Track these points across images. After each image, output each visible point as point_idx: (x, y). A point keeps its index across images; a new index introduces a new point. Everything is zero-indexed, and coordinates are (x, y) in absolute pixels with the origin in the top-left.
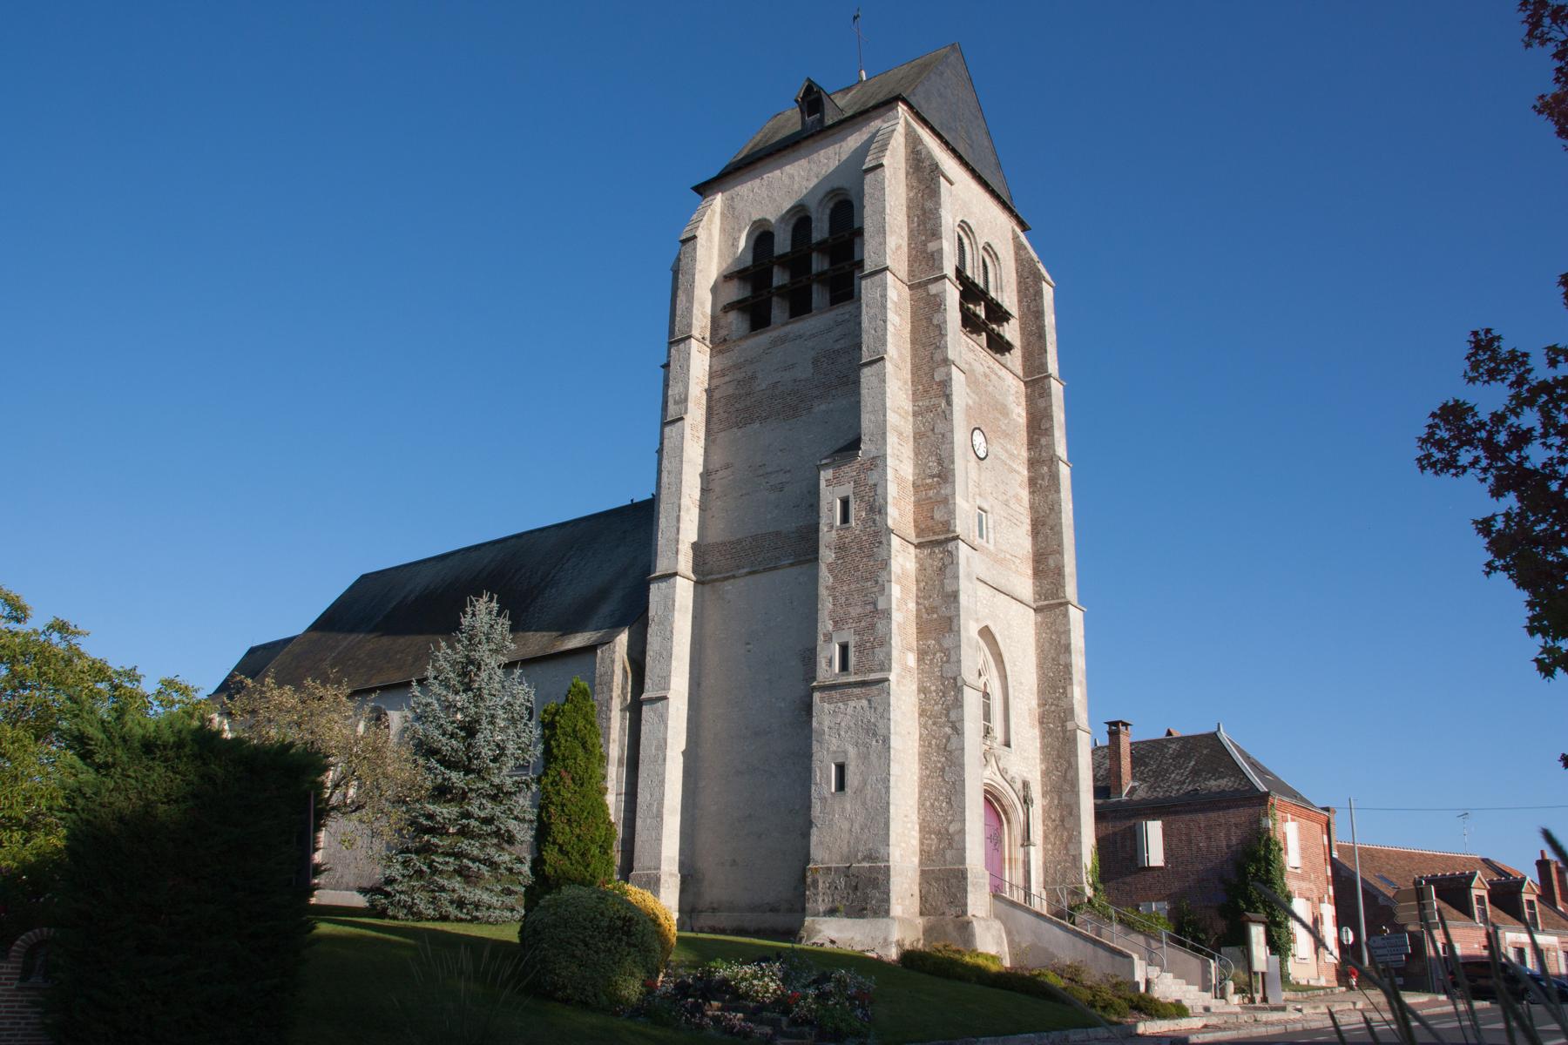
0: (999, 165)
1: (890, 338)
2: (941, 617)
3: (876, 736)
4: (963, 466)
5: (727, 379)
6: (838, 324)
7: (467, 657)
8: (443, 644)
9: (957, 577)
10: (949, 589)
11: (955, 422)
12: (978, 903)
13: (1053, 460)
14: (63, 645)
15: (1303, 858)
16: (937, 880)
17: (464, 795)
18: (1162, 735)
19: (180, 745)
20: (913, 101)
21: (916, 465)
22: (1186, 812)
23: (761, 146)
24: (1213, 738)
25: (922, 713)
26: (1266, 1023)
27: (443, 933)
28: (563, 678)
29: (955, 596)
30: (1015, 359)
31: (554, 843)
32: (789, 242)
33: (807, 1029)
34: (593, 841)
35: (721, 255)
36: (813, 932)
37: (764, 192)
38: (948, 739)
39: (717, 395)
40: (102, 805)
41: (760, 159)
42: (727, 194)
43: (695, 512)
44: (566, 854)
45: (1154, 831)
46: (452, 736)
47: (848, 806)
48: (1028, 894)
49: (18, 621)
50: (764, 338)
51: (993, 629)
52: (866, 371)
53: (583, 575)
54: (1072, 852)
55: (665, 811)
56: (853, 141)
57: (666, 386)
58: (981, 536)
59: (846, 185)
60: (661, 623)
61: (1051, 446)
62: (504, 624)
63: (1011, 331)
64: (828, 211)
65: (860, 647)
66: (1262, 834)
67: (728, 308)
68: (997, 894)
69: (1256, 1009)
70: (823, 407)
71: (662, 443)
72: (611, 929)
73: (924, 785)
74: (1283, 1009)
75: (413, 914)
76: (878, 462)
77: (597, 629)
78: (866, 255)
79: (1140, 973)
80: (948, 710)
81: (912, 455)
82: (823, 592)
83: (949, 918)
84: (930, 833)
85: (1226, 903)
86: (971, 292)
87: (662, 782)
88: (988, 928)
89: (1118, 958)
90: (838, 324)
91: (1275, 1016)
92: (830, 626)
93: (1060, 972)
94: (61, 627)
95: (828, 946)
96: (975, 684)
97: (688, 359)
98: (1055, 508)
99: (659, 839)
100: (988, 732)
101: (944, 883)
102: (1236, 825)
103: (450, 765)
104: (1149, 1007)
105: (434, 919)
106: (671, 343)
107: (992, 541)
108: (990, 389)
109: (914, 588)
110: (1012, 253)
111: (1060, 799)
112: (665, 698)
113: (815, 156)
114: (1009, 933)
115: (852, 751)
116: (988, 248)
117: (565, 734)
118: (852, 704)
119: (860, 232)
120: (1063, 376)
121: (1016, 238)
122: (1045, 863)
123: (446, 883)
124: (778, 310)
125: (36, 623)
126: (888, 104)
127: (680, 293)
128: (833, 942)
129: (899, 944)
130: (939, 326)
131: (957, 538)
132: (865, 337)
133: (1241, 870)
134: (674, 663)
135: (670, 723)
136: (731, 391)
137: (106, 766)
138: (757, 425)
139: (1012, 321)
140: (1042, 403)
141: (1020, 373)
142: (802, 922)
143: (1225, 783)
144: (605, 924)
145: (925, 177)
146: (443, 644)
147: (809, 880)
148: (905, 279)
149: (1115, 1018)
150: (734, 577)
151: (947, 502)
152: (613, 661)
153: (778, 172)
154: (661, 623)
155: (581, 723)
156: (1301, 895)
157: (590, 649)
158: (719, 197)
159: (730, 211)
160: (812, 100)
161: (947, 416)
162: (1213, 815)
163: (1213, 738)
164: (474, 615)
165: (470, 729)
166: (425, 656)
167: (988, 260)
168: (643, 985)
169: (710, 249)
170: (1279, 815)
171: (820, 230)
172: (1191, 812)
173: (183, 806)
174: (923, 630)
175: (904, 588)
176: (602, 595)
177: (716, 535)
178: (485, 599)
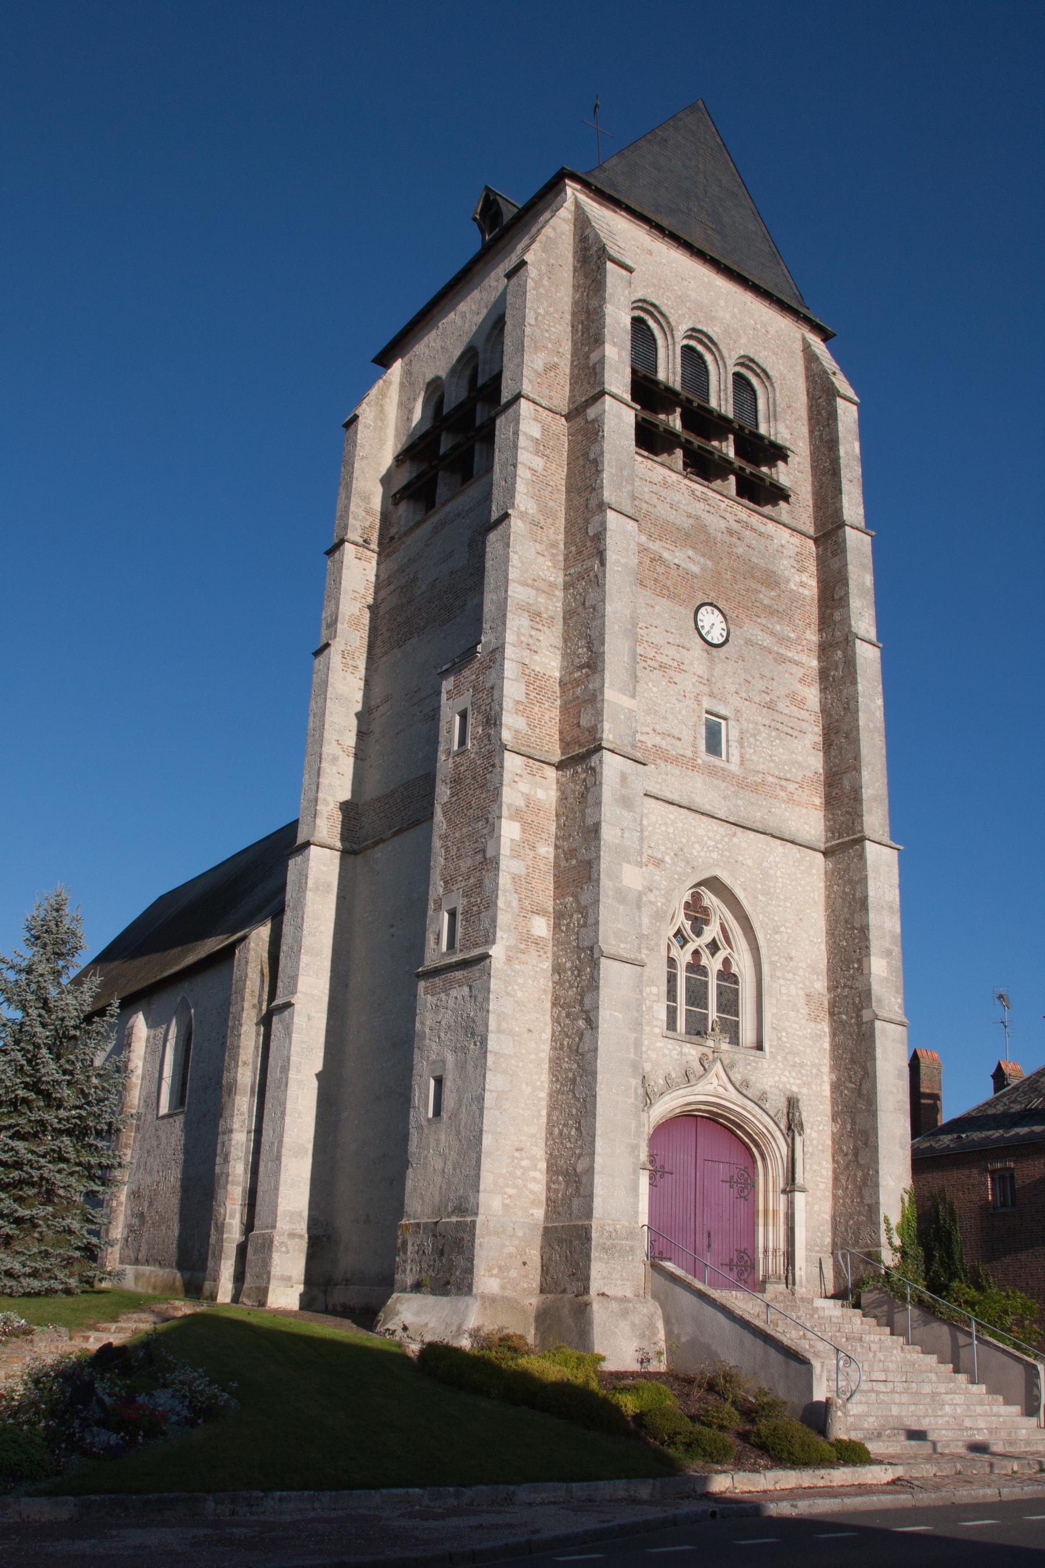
1: (521, 487)
5: (392, 587)
9: (598, 804)
13: (848, 640)
16: (560, 1241)
29: (596, 829)
35: (396, 436)
39: (382, 610)
42: (406, 358)
47: (443, 1137)
54: (867, 1201)
60: (295, 908)
80: (582, 995)
84: (557, 1173)
108: (740, 551)
109: (553, 828)
111: (853, 1123)
113: (486, 283)
115: (450, 1058)
118: (454, 993)
120: (872, 522)
122: (833, 1217)
129: (474, 1334)
138: (415, 640)
140: (834, 563)
153: (452, 315)
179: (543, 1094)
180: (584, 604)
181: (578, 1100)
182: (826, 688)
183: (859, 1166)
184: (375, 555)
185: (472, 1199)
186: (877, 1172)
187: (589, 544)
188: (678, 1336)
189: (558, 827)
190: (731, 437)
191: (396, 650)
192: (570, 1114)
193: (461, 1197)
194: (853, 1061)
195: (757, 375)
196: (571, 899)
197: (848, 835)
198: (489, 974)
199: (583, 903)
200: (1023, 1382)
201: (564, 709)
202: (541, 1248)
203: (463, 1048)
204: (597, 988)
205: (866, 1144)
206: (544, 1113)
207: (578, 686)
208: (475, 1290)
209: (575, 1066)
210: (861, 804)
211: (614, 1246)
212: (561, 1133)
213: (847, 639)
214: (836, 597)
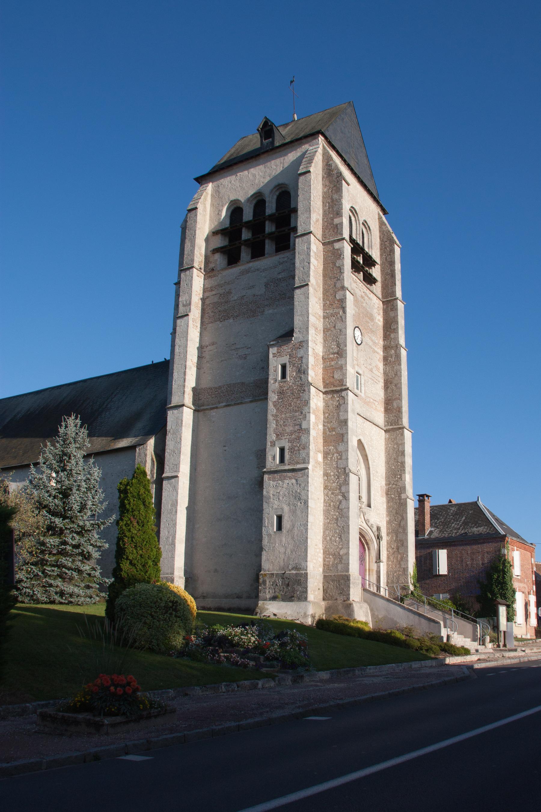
0: (372, 175)
2: (337, 434)
3: (300, 500)
4: (350, 347)
5: (214, 293)
6: (281, 263)
7: (63, 451)
8: (49, 444)
9: (346, 411)
10: (342, 418)
11: (348, 323)
12: (355, 594)
13: (397, 347)
15: (521, 570)
16: (333, 581)
17: (62, 531)
18: (446, 502)
20: (327, 134)
21: (324, 347)
22: (461, 545)
23: (235, 156)
24: (475, 505)
26: (509, 658)
29: (346, 422)
30: (378, 288)
31: (127, 559)
32: (252, 214)
34: (149, 558)
35: (211, 220)
36: (264, 609)
37: (238, 184)
38: (340, 502)
39: (207, 302)
41: (236, 164)
42: (215, 183)
43: (194, 370)
44: (134, 565)
45: (443, 555)
46: (55, 497)
47: (284, 539)
48: (378, 588)
50: (235, 270)
51: (363, 441)
53: (131, 402)
54: (403, 566)
55: (177, 541)
56: (292, 156)
57: (178, 295)
59: (287, 182)
60: (174, 433)
61: (397, 339)
62: (84, 432)
63: (376, 272)
64: (275, 197)
65: (291, 450)
66: (501, 557)
67: (215, 251)
68: (365, 590)
69: (501, 650)
70: (271, 311)
71: (175, 329)
72: (166, 608)
73: (326, 528)
74: (515, 650)
75: (34, 600)
76: (304, 344)
77: (135, 436)
78: (299, 224)
79: (444, 633)
81: (322, 341)
82: (270, 418)
83: (339, 602)
84: (329, 554)
85: (482, 594)
86: (357, 249)
87: (175, 525)
88: (361, 607)
89: (432, 624)
90: (281, 263)
91: (512, 654)
93: (402, 631)
95: (272, 617)
97: (191, 280)
98: (398, 374)
101: (337, 582)
102: (487, 552)
103: (54, 514)
104: (451, 650)
105: (46, 603)
106: (182, 270)
107: (363, 391)
108: (364, 305)
110: (378, 227)
111: (397, 537)
113: (268, 164)
114: (372, 610)
115: (286, 508)
116: (365, 223)
117: (133, 496)
118: (286, 481)
119: (295, 210)
121: (380, 218)
122: (387, 572)
123: (52, 582)
124: (245, 254)
126: (313, 135)
127: (187, 241)
128: (275, 615)
129: (313, 617)
131: (348, 389)
132: (297, 272)
133: (489, 576)
136: (216, 299)
138: (231, 321)
139: (377, 266)
141: (380, 297)
142: (257, 605)
143: (482, 530)
144: (163, 605)
146: (49, 444)
147: (261, 581)
148: (321, 239)
149: (433, 656)
150: (217, 408)
151: (342, 368)
152: (146, 455)
153: (246, 172)
154: (174, 433)
155: (142, 491)
156: (520, 591)
157: (132, 448)
158: (210, 185)
159: (217, 193)
160: (267, 130)
161: (343, 320)
162: (475, 547)
163: (475, 505)
164: (66, 427)
165: (65, 494)
167: (364, 230)
168: (184, 639)
169: (205, 215)
170: (510, 547)
171: (271, 208)
174: (326, 441)
175: (316, 417)
176: (137, 416)
177: (206, 383)
178: (73, 418)
179: (321, 524)
180: (335, 327)
181: (340, 527)
182: (386, 364)
183: (399, 553)
184: (203, 275)
185: (303, 564)
186: (407, 556)
187: (336, 302)
188: (377, 616)
190: (361, 255)
191: (218, 323)
192: (335, 532)
193: (296, 563)
194: (397, 513)
195: (366, 228)
196: (333, 448)
197: (395, 425)
198: (308, 476)
199: (339, 450)
200: (472, 631)
201: (325, 369)
202: (323, 583)
204: (348, 484)
205: (402, 545)
206: (322, 531)
207: (332, 361)
208: (308, 600)
209: (338, 513)
210: (402, 414)
211: (355, 582)
213: (397, 346)
214: (392, 328)
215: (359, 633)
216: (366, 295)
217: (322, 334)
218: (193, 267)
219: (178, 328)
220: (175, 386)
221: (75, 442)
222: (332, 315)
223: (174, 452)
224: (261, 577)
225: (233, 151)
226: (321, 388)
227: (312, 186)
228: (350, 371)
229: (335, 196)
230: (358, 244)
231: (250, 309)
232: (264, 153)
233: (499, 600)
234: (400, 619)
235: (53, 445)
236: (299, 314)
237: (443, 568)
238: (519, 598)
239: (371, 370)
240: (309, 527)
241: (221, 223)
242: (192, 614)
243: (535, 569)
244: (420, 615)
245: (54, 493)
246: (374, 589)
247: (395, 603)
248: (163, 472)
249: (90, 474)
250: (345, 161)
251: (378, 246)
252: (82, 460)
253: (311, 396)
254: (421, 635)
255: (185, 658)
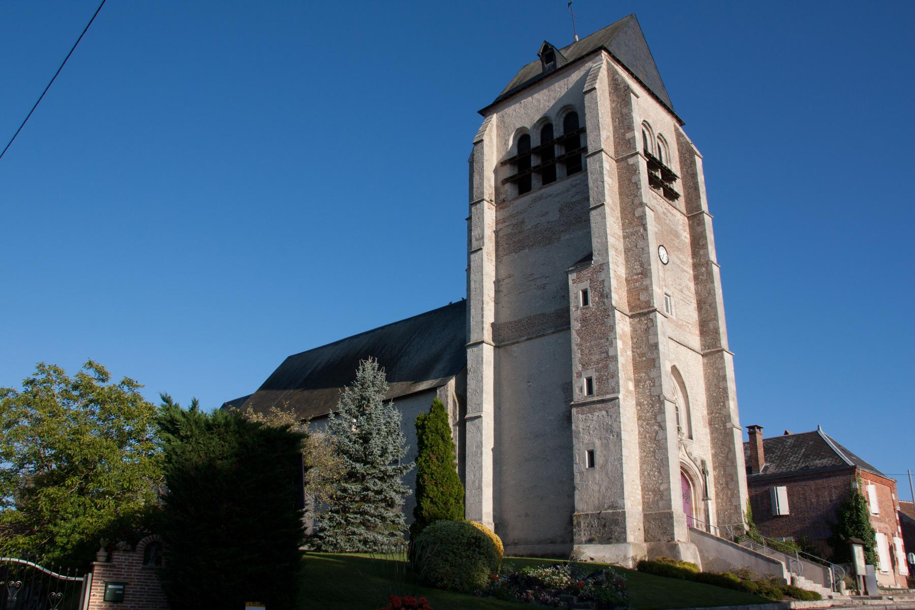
0: (663, 86)
2: (648, 359)
3: (613, 433)
4: (655, 267)
5: (507, 224)
7: (361, 395)
9: (656, 334)
10: (652, 342)
12: (681, 533)
13: (708, 263)
14: (130, 394)
16: (654, 519)
17: (363, 477)
18: (782, 434)
19: (227, 424)
20: (610, 49)
21: (627, 268)
23: (518, 84)
24: (815, 435)
25: (639, 418)
27: (357, 557)
28: (420, 409)
29: (656, 346)
30: (681, 203)
31: (428, 497)
32: (539, 140)
33: (590, 603)
34: (450, 495)
38: (657, 433)
39: (501, 234)
40: (186, 460)
42: (500, 114)
45: (782, 493)
46: (355, 443)
48: (708, 528)
49: (103, 381)
50: (527, 198)
51: (678, 367)
52: (593, 213)
53: (430, 345)
54: (734, 504)
57: (470, 230)
58: (667, 311)
60: (475, 372)
62: (382, 375)
63: (677, 186)
64: (562, 120)
65: (599, 379)
68: (691, 528)
69: (861, 598)
70: (567, 237)
71: (469, 265)
72: (469, 544)
73: (643, 462)
74: (880, 598)
76: (604, 267)
77: (435, 378)
79: (787, 575)
80: (656, 416)
82: (574, 347)
83: (663, 543)
84: (648, 491)
85: (835, 535)
86: (654, 164)
88: (688, 548)
89: (772, 565)
92: (580, 368)
93: (737, 573)
94: (129, 383)
95: (589, 561)
96: (671, 399)
98: (711, 293)
99: (480, 502)
100: (679, 429)
101: (659, 521)
102: (835, 487)
103: (357, 460)
106: (472, 205)
107: (674, 314)
110: (675, 139)
111: (725, 471)
112: (480, 417)
114: (701, 551)
115: (598, 443)
116: (660, 137)
118: (596, 414)
119: (584, 130)
121: (676, 130)
122: (717, 511)
123: (356, 530)
124: (536, 181)
125: (114, 380)
126: (596, 51)
127: (475, 174)
128: (592, 559)
129: (634, 559)
130: (636, 183)
131: (655, 310)
132: (591, 192)
133: (840, 516)
134: (484, 396)
135: (484, 432)
136: (509, 231)
137: (187, 437)
138: (527, 251)
139: (678, 180)
141: (685, 212)
143: (826, 462)
144: (465, 541)
145: (622, 95)
147: (575, 522)
148: (613, 156)
149: (775, 600)
150: (518, 342)
151: (648, 289)
152: (447, 396)
153: (530, 99)
154: (475, 372)
155: (440, 425)
156: (880, 531)
157: (433, 390)
158: (495, 116)
159: (502, 124)
160: (548, 54)
161: (644, 237)
162: (819, 481)
164: (364, 370)
165: (365, 439)
166: (333, 400)
167: (661, 144)
169: (491, 147)
170: (863, 480)
172: (805, 480)
173: (230, 461)
174: (637, 368)
175: (624, 342)
176: (436, 359)
177: (505, 317)
189: (633, 343)
192: (654, 466)
201: (629, 291)
203: (606, 438)
205: (732, 480)
212: (649, 474)
215: (687, 575)
216: (668, 210)
217: (623, 255)
218: (483, 200)
219: (472, 263)
220: (472, 323)
221: (373, 385)
222: (633, 234)
223: (476, 391)
224: (574, 518)
225: (515, 80)
226: (627, 311)
227: (599, 104)
228: (658, 292)
229: (625, 111)
230: (655, 159)
231: (545, 237)
232: (546, 77)
233: (853, 539)
234: (734, 561)
235: (352, 390)
236: (597, 235)
237: (783, 507)
238: (881, 541)
239: (681, 291)
240: (624, 461)
241: (509, 153)
242: (498, 553)
243: (898, 508)
244: (757, 555)
245: (354, 438)
246: (704, 530)
247: (726, 543)
248: (465, 413)
249: (389, 417)
250: (632, 74)
251: (677, 159)
252: (381, 404)
253: (617, 321)
254: (760, 577)
255: (490, 597)
